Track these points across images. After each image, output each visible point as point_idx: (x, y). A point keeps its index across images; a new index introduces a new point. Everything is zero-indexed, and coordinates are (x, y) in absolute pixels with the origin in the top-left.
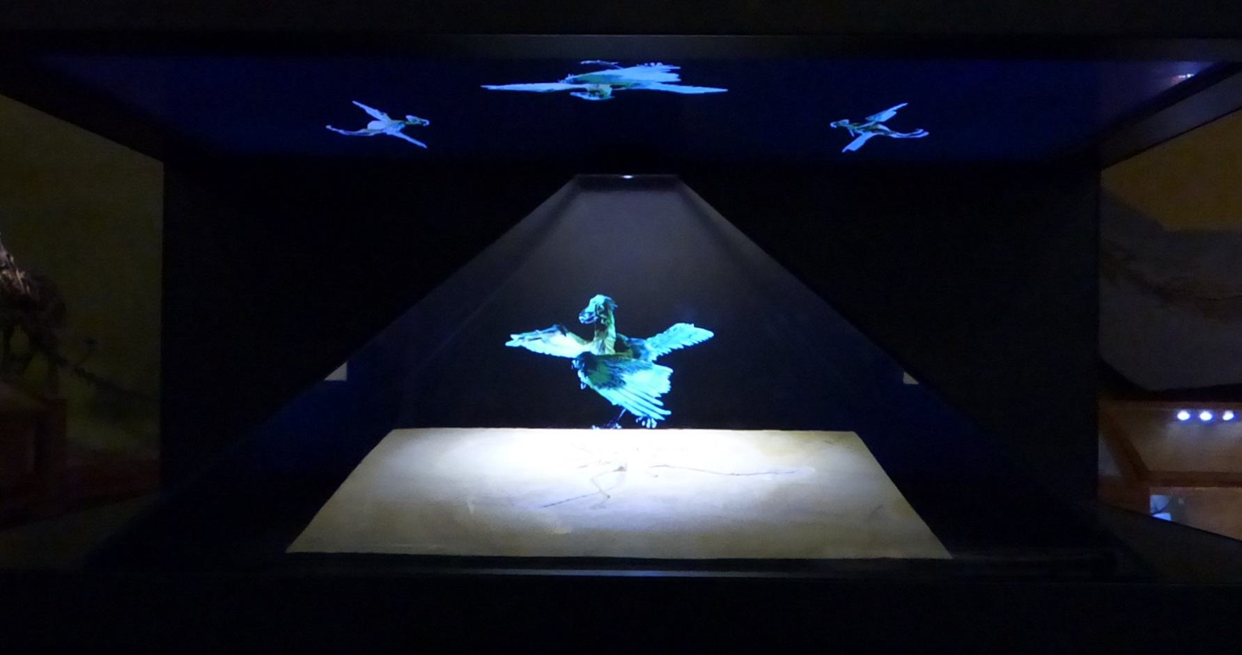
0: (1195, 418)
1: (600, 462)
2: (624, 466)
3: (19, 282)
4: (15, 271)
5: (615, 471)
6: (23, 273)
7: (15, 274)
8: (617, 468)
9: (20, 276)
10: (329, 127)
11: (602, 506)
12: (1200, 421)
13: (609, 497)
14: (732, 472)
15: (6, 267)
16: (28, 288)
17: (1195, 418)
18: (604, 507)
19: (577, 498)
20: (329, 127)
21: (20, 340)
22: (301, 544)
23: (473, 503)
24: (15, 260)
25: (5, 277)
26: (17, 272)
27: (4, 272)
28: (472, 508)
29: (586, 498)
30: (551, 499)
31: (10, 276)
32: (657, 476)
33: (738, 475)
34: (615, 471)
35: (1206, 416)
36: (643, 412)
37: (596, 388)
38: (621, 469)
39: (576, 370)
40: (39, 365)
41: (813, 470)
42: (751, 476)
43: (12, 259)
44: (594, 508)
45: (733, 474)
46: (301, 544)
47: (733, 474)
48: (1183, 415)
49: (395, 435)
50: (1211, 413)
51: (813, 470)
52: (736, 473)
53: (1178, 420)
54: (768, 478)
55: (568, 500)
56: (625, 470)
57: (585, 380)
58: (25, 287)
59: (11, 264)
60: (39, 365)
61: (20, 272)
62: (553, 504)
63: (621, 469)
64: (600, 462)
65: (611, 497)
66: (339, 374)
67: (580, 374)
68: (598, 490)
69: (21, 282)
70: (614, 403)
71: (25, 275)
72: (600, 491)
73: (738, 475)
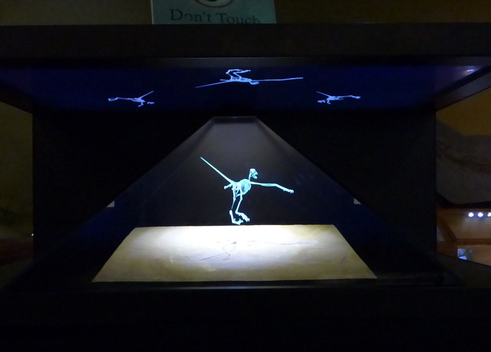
0: (476, 216)
5: (232, 244)
8: (233, 243)
12: (478, 217)
13: (230, 255)
17: (476, 216)
18: (228, 260)
19: (216, 256)
22: (98, 278)
29: (213, 258)
32: (250, 246)
33: (284, 244)
34: (232, 244)
35: (480, 215)
38: (234, 243)
42: (290, 245)
44: (224, 259)
45: (282, 244)
46: (98, 278)
47: (282, 244)
48: (471, 215)
49: (136, 231)
53: (469, 217)
54: (298, 245)
55: (212, 257)
62: (206, 259)
65: (231, 255)
66: (112, 205)
72: (226, 253)
73: (284, 244)
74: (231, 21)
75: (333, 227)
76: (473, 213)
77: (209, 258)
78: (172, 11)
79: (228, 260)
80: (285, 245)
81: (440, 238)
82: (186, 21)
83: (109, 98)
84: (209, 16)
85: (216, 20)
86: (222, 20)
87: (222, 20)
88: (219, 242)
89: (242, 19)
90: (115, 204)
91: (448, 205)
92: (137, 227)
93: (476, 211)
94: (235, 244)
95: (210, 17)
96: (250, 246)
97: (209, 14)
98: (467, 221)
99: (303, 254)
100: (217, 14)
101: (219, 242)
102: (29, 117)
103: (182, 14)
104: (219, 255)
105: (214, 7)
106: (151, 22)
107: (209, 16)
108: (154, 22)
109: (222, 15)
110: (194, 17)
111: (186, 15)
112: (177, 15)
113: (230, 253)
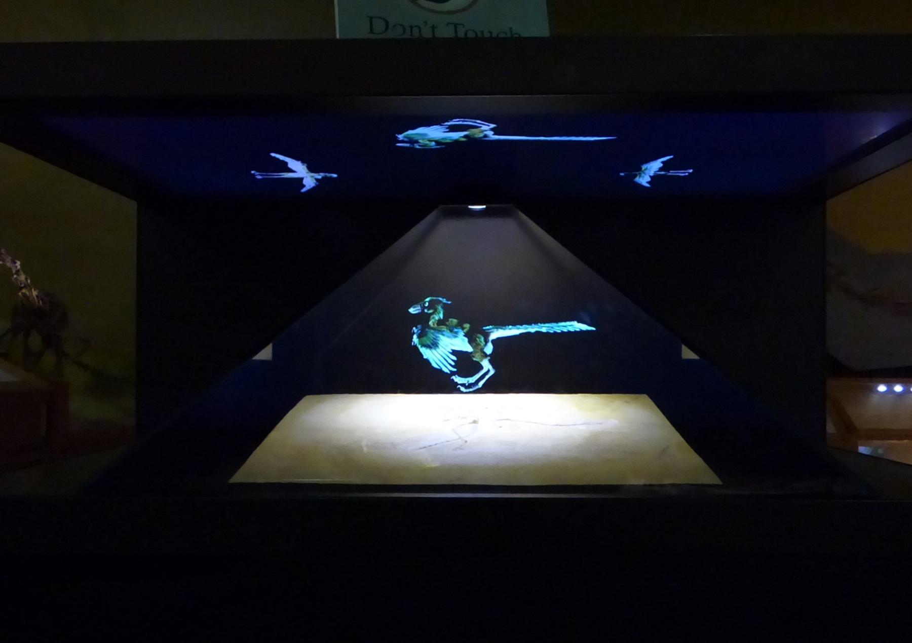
0: (890, 391)
1: (459, 417)
2: (477, 420)
3: (34, 298)
4: (31, 289)
5: (470, 423)
6: (37, 291)
7: (32, 292)
8: (472, 421)
9: (35, 293)
10: (335, 176)
11: (460, 448)
12: (894, 392)
13: (466, 442)
14: (556, 424)
15: (25, 287)
16: (41, 302)
17: (890, 391)
18: (462, 449)
19: (442, 443)
20: (335, 176)
21: (35, 341)
22: (240, 477)
23: (367, 446)
24: (31, 281)
25: (24, 294)
26: (33, 290)
27: (24, 291)
28: (365, 449)
29: (437, 446)
30: (424, 444)
31: (28, 293)
32: (501, 427)
33: (561, 425)
34: (470, 423)
35: (898, 388)
36: (440, 366)
37: (419, 347)
38: (475, 422)
39: (414, 333)
40: (49, 359)
41: (616, 422)
42: (571, 427)
43: (29, 281)
44: (455, 449)
45: (557, 425)
46: (240, 477)
47: (557, 425)
48: (882, 388)
49: (307, 401)
50: (902, 386)
51: (616, 422)
52: (560, 424)
53: (878, 391)
54: (583, 427)
55: (436, 444)
56: (477, 423)
57: (415, 339)
58: (39, 302)
59: (29, 285)
60: (49, 359)
61: (35, 290)
62: (425, 447)
63: (475, 422)
64: (459, 417)
65: (468, 442)
66: (266, 354)
67: (415, 337)
68: (458, 437)
69: (35, 298)
70: (425, 357)
71: (38, 293)
72: (460, 438)
73: (561, 425)
74: (471, 35)
75: (645, 398)
76: (885, 385)
77: (430, 446)
78: (371, 18)
79: (462, 449)
80: (560, 427)
81: (830, 428)
82: (395, 34)
83: (409, 308)
84: (433, 27)
85: (445, 32)
86: (456, 31)
87: (456, 31)
88: (448, 420)
89: (491, 33)
90: (275, 352)
91: (840, 370)
92: (309, 394)
93: (890, 382)
94: (474, 424)
95: (436, 30)
96: (501, 427)
97: (433, 25)
98: (874, 399)
99: (593, 442)
100: (448, 24)
101: (448, 420)
102: (130, 207)
103: (387, 23)
104: (448, 441)
105: (442, 13)
106: (335, 34)
107: (433, 27)
108: (340, 35)
109: (456, 25)
110: (408, 30)
111: (395, 26)
112: (379, 26)
113: (467, 440)
